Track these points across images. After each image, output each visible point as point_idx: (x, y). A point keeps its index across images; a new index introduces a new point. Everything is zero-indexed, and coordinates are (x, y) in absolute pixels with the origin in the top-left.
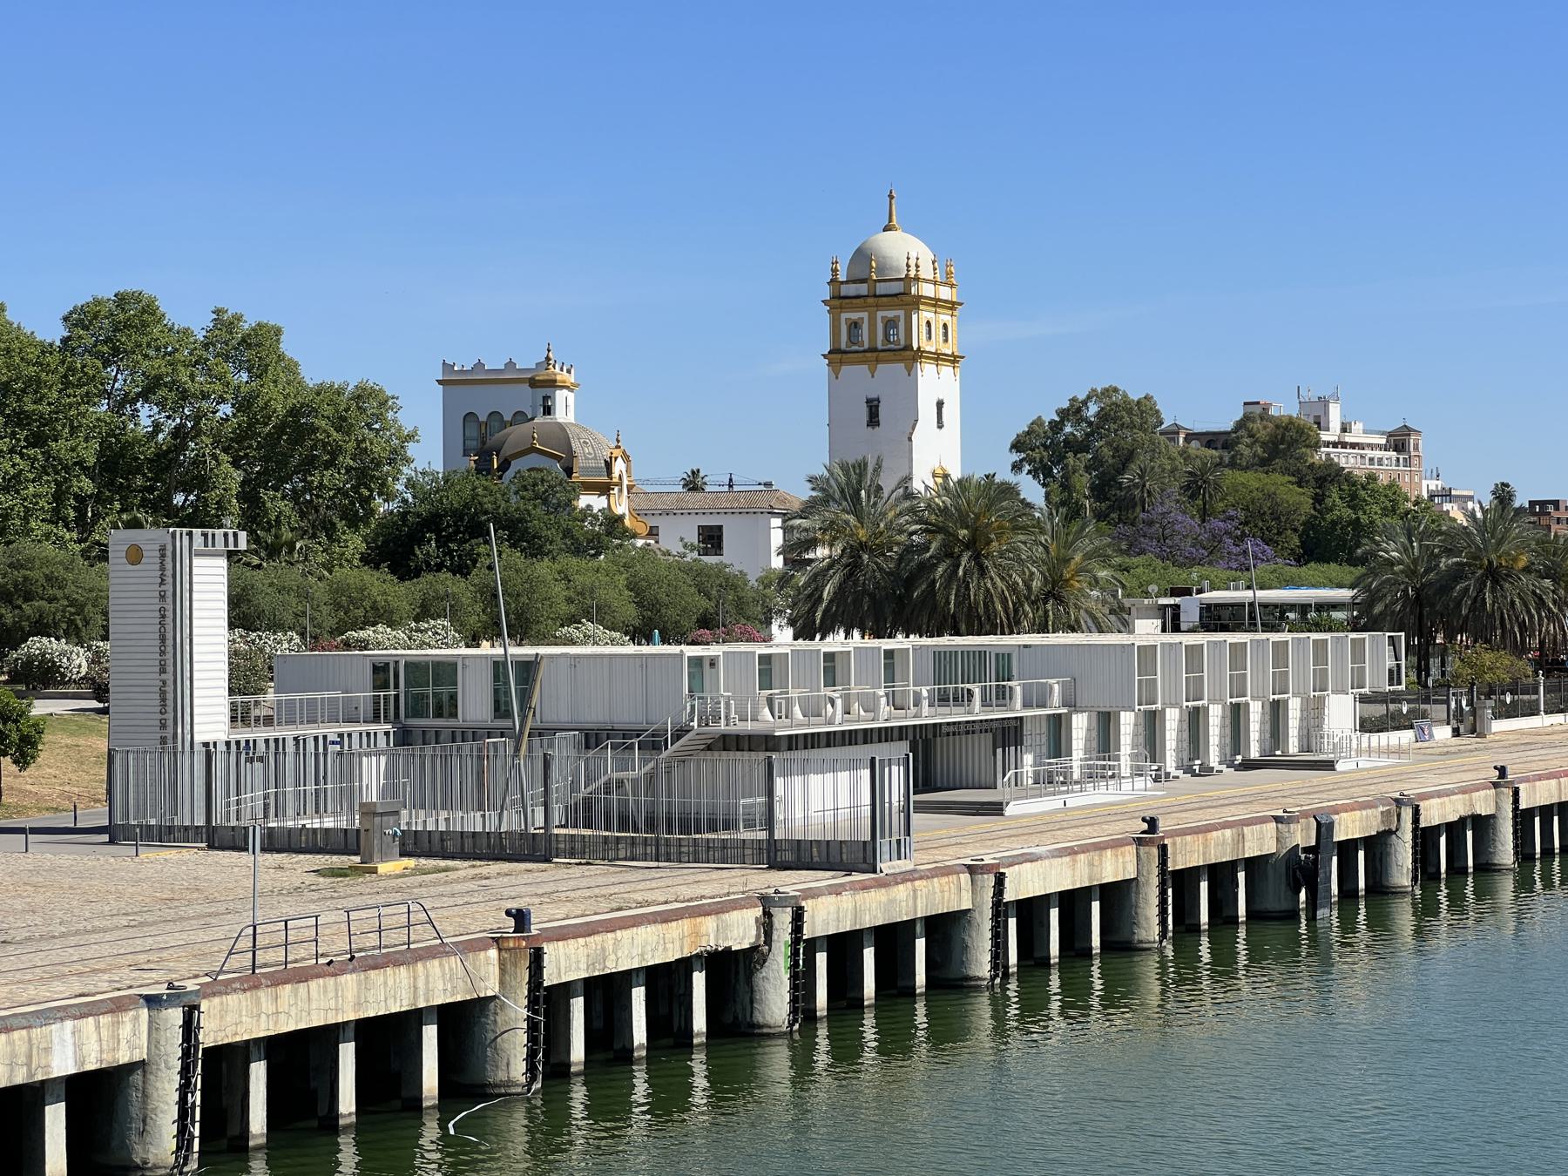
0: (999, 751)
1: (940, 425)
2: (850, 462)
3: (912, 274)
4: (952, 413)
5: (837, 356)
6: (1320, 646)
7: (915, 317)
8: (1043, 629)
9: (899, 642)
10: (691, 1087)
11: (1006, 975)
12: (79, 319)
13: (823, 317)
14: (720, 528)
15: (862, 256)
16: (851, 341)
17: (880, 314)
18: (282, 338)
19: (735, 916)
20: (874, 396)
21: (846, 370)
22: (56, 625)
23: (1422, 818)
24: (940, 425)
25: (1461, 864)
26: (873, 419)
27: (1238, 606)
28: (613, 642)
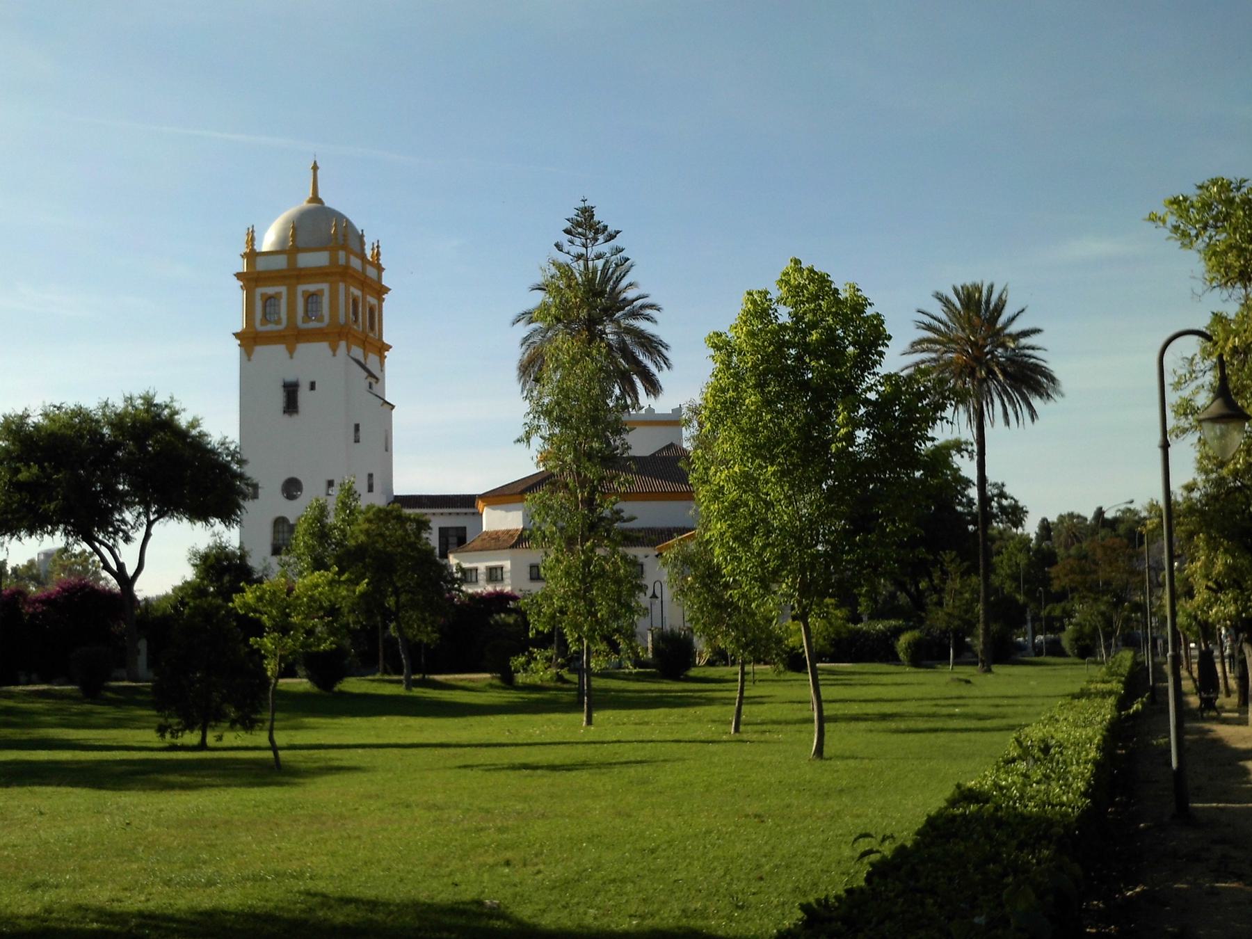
0: (1224, 715)
1: (371, 476)
2: (136, 395)
5: (249, 340)
6: (811, 721)
8: (28, 684)
9: (490, 588)
10: (490, 594)
11: (61, 710)
12: (1061, 518)
13: (236, 296)
14: (441, 529)
15: (959, 786)
16: (265, 319)
17: (301, 288)
18: (841, 283)
19: (974, 464)
20: (290, 378)
21: (261, 351)
22: (687, 561)
23: (832, 725)
24: (371, 476)
25: (23, 679)
26: (291, 405)
27: (638, 680)
28: (462, 680)
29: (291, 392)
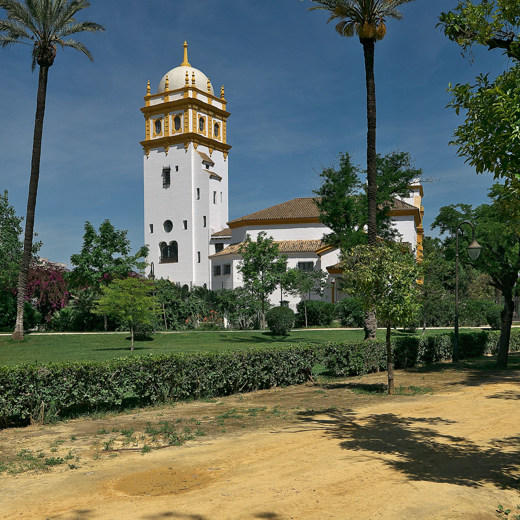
20: (166, 166)
29: (166, 173)
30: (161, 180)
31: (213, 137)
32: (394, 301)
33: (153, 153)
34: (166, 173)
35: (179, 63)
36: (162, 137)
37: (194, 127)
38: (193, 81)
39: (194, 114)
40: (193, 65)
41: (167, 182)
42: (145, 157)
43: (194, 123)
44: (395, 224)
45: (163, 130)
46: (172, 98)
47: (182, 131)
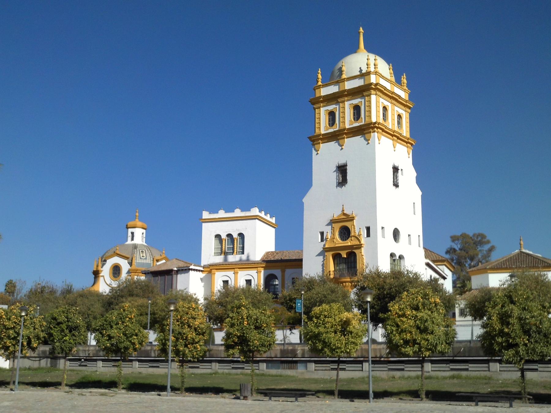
3: (372, 69)
4: (409, 174)
7: (373, 97)
20: (342, 162)
29: (342, 170)
30: (334, 177)
31: (396, 129)
32: (524, 342)
33: (324, 147)
34: (342, 170)
35: (355, 49)
36: (363, 123)
37: (377, 116)
38: (375, 65)
39: (377, 102)
40: (370, 49)
41: (343, 181)
42: (314, 153)
43: (377, 111)
44: (410, 243)
45: (337, 122)
46: (348, 85)
47: (336, 128)
